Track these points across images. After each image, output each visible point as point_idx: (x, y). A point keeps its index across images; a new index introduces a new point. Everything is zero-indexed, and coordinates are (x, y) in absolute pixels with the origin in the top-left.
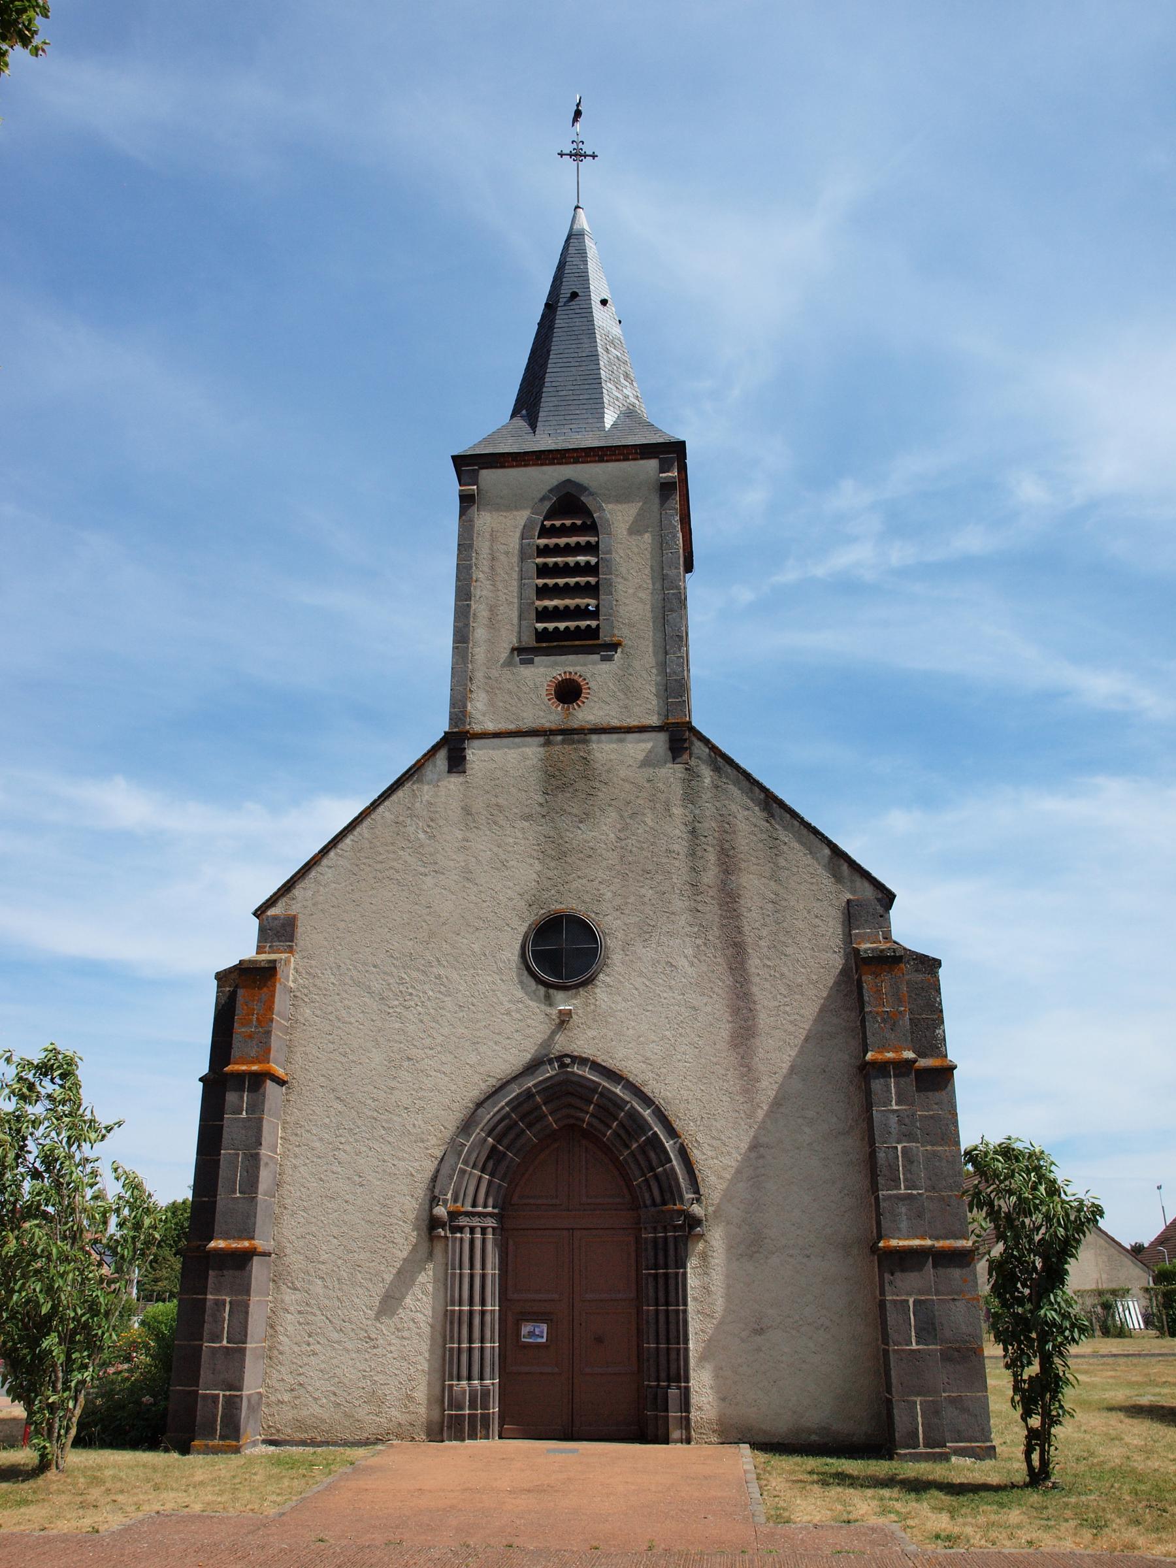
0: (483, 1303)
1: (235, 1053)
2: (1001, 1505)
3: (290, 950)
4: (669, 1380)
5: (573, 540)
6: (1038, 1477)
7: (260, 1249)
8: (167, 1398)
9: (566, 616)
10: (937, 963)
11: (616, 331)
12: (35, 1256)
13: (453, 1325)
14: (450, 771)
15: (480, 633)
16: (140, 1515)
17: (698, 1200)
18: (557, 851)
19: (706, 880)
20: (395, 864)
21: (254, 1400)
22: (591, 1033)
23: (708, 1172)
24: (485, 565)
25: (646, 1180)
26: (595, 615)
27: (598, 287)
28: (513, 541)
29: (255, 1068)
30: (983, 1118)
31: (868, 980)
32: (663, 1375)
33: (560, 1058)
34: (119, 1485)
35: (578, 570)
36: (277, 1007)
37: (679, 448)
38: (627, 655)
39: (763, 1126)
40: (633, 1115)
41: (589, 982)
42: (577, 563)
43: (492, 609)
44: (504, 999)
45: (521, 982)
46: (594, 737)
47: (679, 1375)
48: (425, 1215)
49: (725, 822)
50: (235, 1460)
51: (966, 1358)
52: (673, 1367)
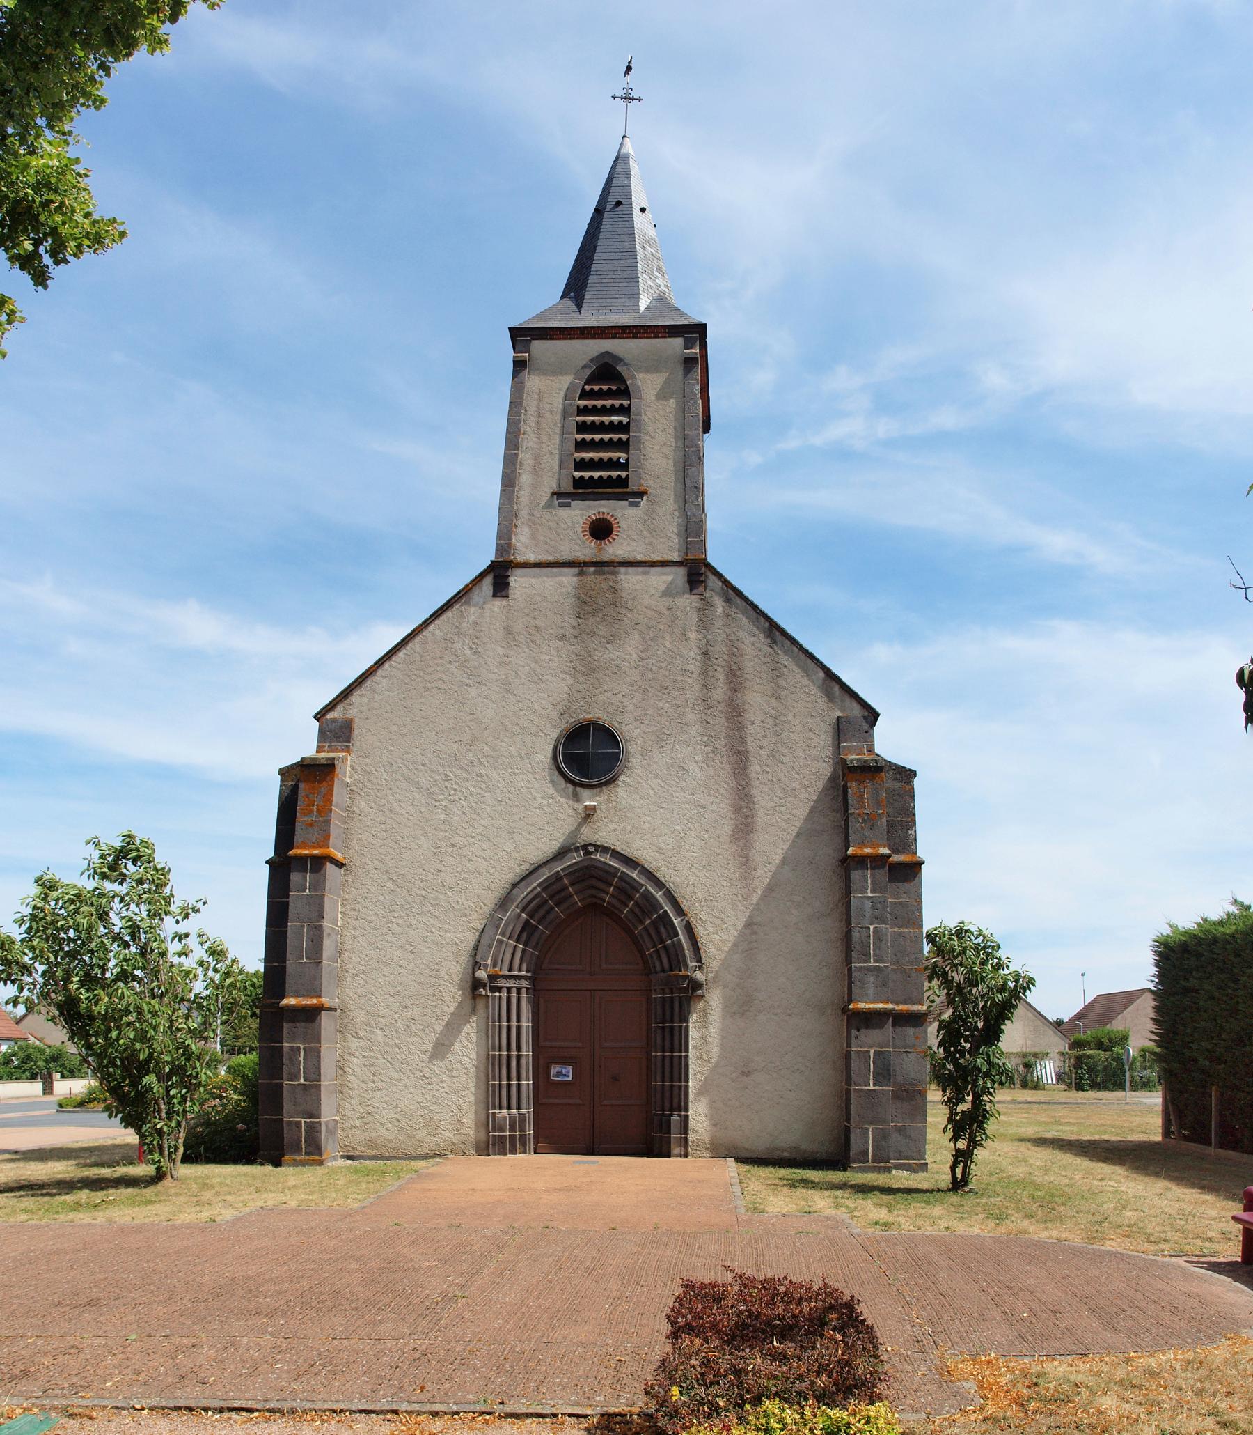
0: (519, 1049)
1: (298, 839)
2: (928, 1203)
3: (347, 749)
4: (672, 1110)
5: (608, 403)
6: (959, 1184)
7: (327, 1005)
8: (257, 1125)
9: (600, 467)
10: (912, 774)
11: (652, 233)
12: (127, 1012)
13: (495, 1067)
14: (494, 595)
15: (525, 478)
16: (248, 1209)
17: (700, 967)
18: (586, 668)
19: (715, 697)
20: (443, 676)
21: (331, 1125)
22: (612, 826)
23: (709, 945)
24: (532, 420)
25: (657, 952)
26: (625, 467)
27: (639, 198)
28: (557, 402)
29: (316, 852)
30: (942, 905)
31: (853, 786)
32: (667, 1105)
33: (585, 847)
34: (226, 1189)
35: (612, 428)
36: (335, 799)
38: (652, 502)
39: (757, 908)
40: (647, 896)
41: (613, 781)
42: (611, 422)
43: (536, 459)
44: (538, 796)
45: (552, 781)
46: (622, 570)
47: (679, 1104)
48: (469, 979)
49: (735, 652)
50: (319, 1171)
51: (913, 1097)
52: (675, 1101)
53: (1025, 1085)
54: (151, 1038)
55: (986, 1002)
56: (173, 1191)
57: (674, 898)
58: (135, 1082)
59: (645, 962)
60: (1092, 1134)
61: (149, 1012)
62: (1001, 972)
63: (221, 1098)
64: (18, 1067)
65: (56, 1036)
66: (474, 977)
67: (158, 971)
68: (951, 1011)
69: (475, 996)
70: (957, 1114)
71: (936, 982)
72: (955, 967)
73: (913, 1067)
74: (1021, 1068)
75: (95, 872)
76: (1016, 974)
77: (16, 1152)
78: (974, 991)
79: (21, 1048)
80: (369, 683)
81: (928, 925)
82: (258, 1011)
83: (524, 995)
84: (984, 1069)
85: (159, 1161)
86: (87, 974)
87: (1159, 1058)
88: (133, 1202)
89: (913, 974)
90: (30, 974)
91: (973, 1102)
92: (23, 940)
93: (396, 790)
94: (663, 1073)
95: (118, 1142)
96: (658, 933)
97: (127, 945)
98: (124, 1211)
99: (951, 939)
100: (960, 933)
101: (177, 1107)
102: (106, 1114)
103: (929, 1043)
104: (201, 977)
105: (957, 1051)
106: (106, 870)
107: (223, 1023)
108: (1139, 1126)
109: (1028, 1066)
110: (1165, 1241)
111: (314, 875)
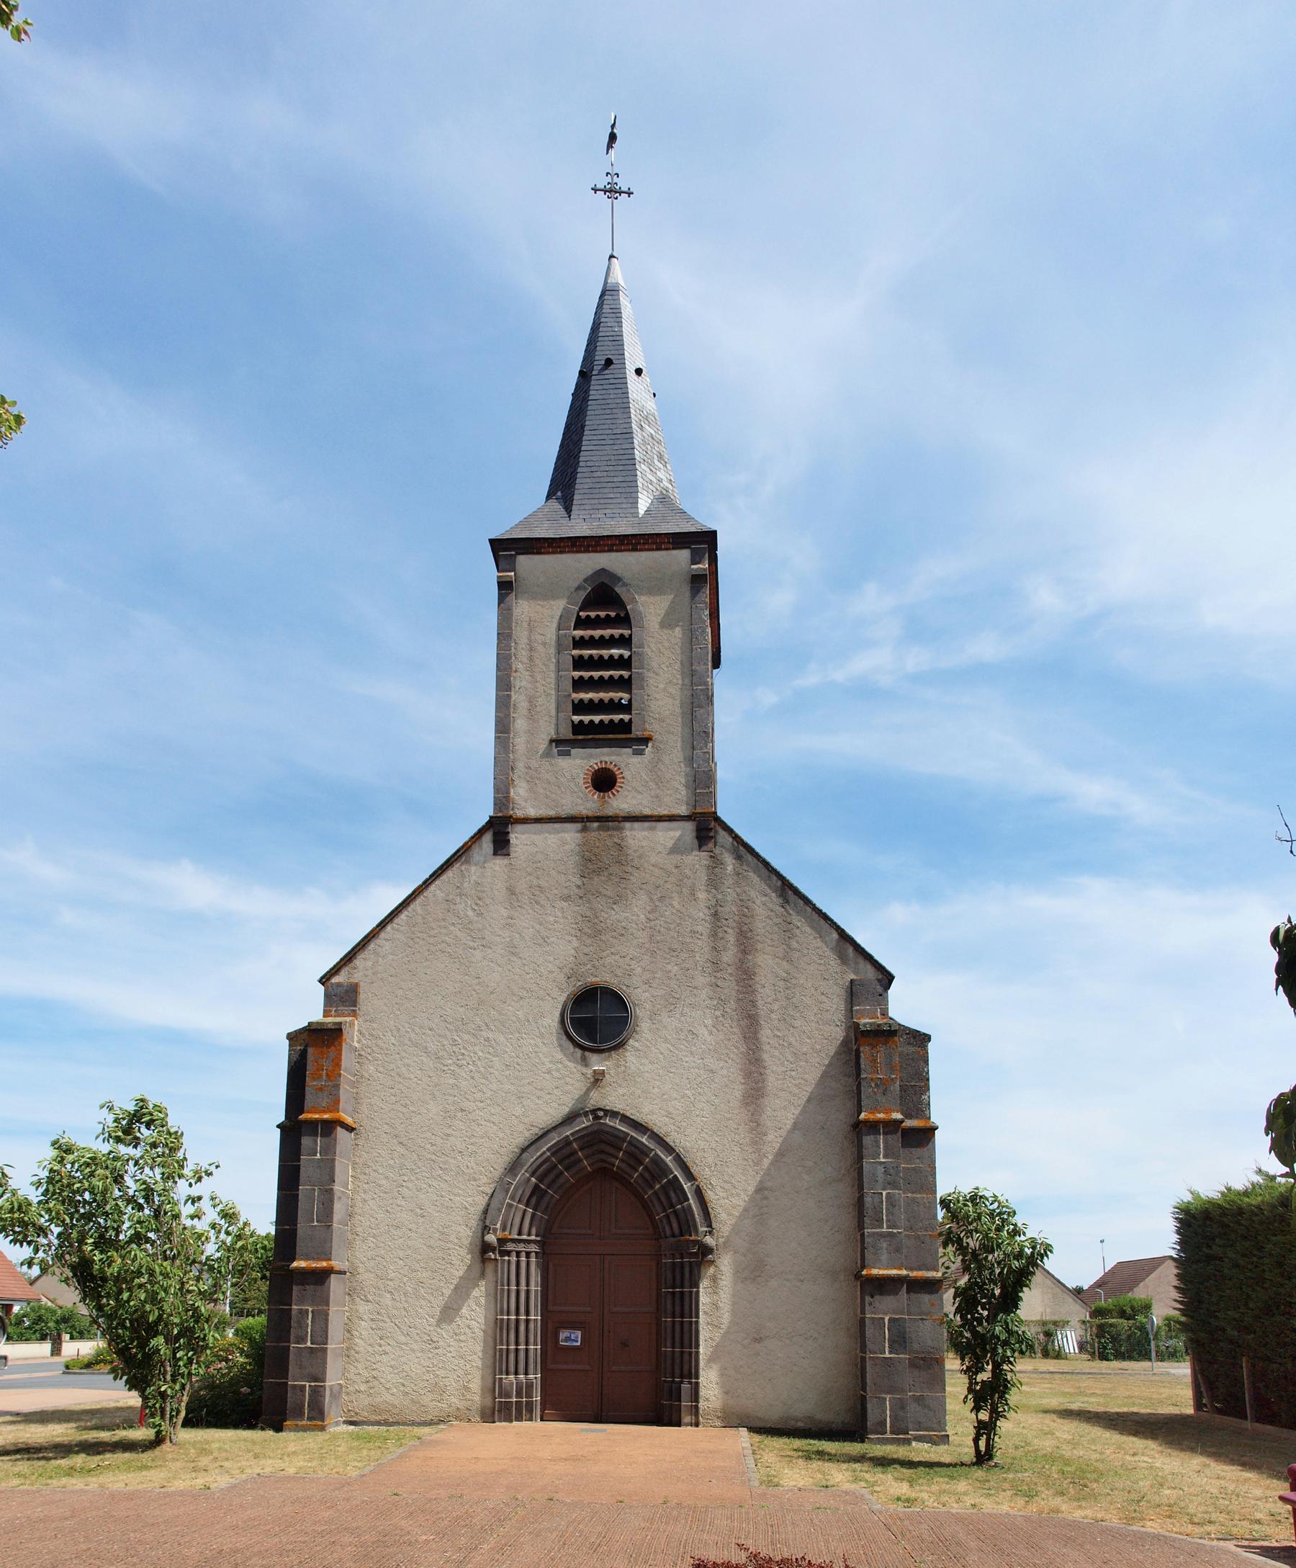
2: (952, 1478)
4: (682, 1376)
6: (983, 1458)
8: (262, 1389)
9: (601, 713)
10: (927, 1038)
11: (651, 405)
12: (139, 1274)
13: (503, 1331)
14: (495, 854)
15: (520, 724)
17: (710, 1232)
18: (592, 930)
21: (336, 1389)
22: (621, 1091)
25: (667, 1216)
26: (627, 708)
27: (633, 355)
29: (326, 1116)
30: (957, 1170)
31: (865, 1050)
32: (677, 1371)
33: (594, 1111)
39: (768, 1173)
40: (657, 1161)
41: (621, 1045)
42: (611, 656)
43: (531, 700)
45: (560, 1045)
46: (628, 825)
47: (691, 1372)
48: (479, 1243)
49: (745, 914)
50: (320, 1436)
51: (930, 1366)
52: (686, 1367)
53: (1046, 1354)
54: (162, 1300)
55: (1003, 1269)
56: (170, 1456)
57: (684, 1163)
58: (143, 1344)
59: (655, 1227)
60: (1120, 1407)
61: (161, 1274)
62: (1017, 1238)
63: (227, 1360)
64: (29, 1328)
65: (68, 1297)
66: (483, 1241)
67: (171, 1234)
68: (967, 1278)
69: (484, 1260)
70: (977, 1383)
71: (950, 1248)
72: (970, 1233)
73: (930, 1334)
74: (1041, 1337)
75: (110, 1136)
76: (1033, 1240)
77: (18, 1414)
78: (990, 1257)
79: (33, 1310)
80: (372, 946)
81: (942, 1190)
82: (268, 1274)
83: (533, 1259)
84: (1003, 1337)
85: (160, 1425)
86: (102, 1236)
87: (1185, 1327)
88: (128, 1467)
89: (928, 1240)
90: (46, 1236)
91: (993, 1371)
92: (40, 1202)
93: (404, 1054)
94: (673, 1338)
95: (120, 1404)
96: (668, 1197)
97: (141, 1208)
98: (118, 1477)
99: (965, 1205)
100: (975, 1198)
101: (183, 1370)
102: (112, 1376)
103: (945, 1310)
104: (213, 1239)
105: (974, 1319)
106: (120, 1134)
107: (233, 1285)
108: (1169, 1397)
109: (1048, 1334)
110: (1210, 1522)
111: (326, 1139)
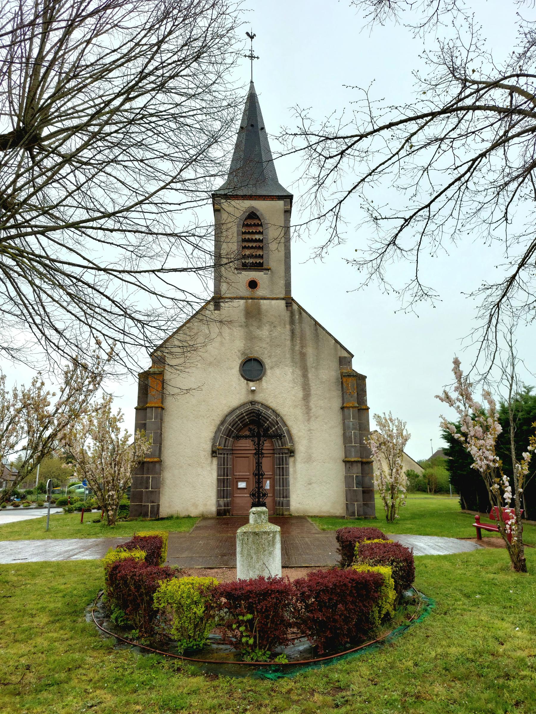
10: (366, 377)
18: (250, 338)
35: (256, 241)
37: (291, 197)
38: (272, 272)
